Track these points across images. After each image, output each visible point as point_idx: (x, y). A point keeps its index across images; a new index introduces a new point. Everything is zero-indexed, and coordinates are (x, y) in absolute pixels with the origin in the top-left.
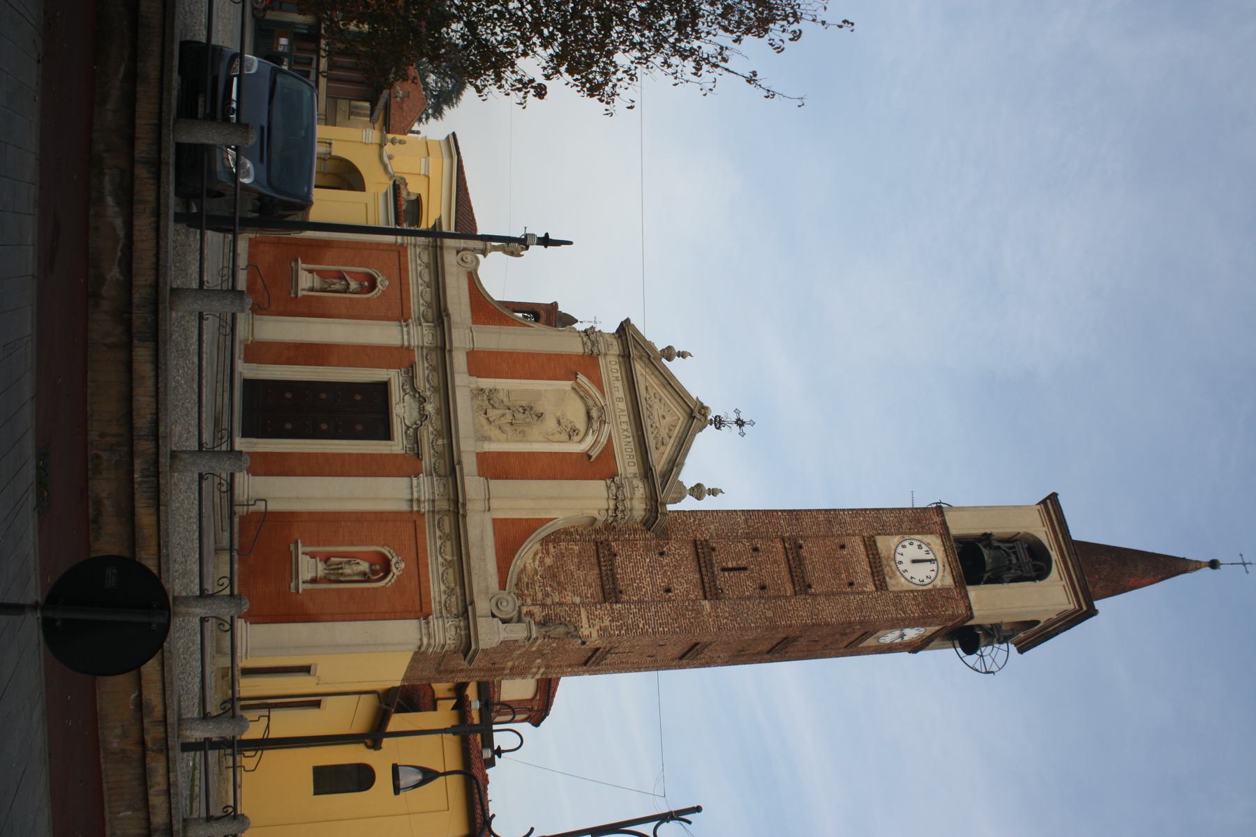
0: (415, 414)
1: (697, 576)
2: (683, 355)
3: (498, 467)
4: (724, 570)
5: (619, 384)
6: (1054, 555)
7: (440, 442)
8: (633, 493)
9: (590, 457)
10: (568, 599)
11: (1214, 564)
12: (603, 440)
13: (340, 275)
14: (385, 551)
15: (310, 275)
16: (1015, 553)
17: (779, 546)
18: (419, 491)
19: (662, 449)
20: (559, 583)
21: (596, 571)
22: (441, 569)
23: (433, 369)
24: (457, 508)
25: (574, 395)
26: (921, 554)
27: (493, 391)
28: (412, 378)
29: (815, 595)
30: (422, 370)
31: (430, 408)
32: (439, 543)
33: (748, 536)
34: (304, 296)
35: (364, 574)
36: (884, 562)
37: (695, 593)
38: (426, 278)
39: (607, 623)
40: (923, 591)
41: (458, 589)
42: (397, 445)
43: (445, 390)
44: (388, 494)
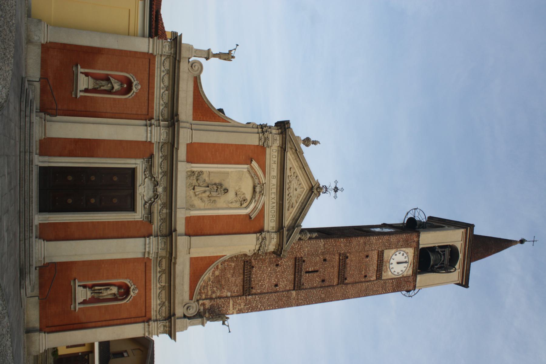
0: (151, 194)
1: (293, 277)
2: (315, 143)
3: (199, 228)
4: (307, 272)
5: (275, 166)
6: (461, 256)
7: (165, 211)
8: (270, 242)
9: (250, 218)
10: (224, 294)
11: (522, 241)
12: (260, 207)
13: (107, 79)
14: (127, 282)
15: (86, 78)
16: (444, 254)
17: (337, 258)
18: (149, 247)
19: (291, 210)
20: (221, 285)
21: (242, 277)
22: (158, 291)
23: (165, 157)
24: (171, 257)
25: (248, 175)
26: (403, 259)
27: (201, 173)
28: (150, 167)
29: (347, 284)
30: (157, 160)
31: (160, 190)
32: (158, 275)
33: (323, 253)
34: (81, 96)
35: (114, 294)
36: (384, 264)
37: (290, 286)
38: (166, 83)
39: (242, 307)
40: (397, 278)
41: (167, 303)
42: (138, 215)
43: (171, 174)
44: (131, 248)
